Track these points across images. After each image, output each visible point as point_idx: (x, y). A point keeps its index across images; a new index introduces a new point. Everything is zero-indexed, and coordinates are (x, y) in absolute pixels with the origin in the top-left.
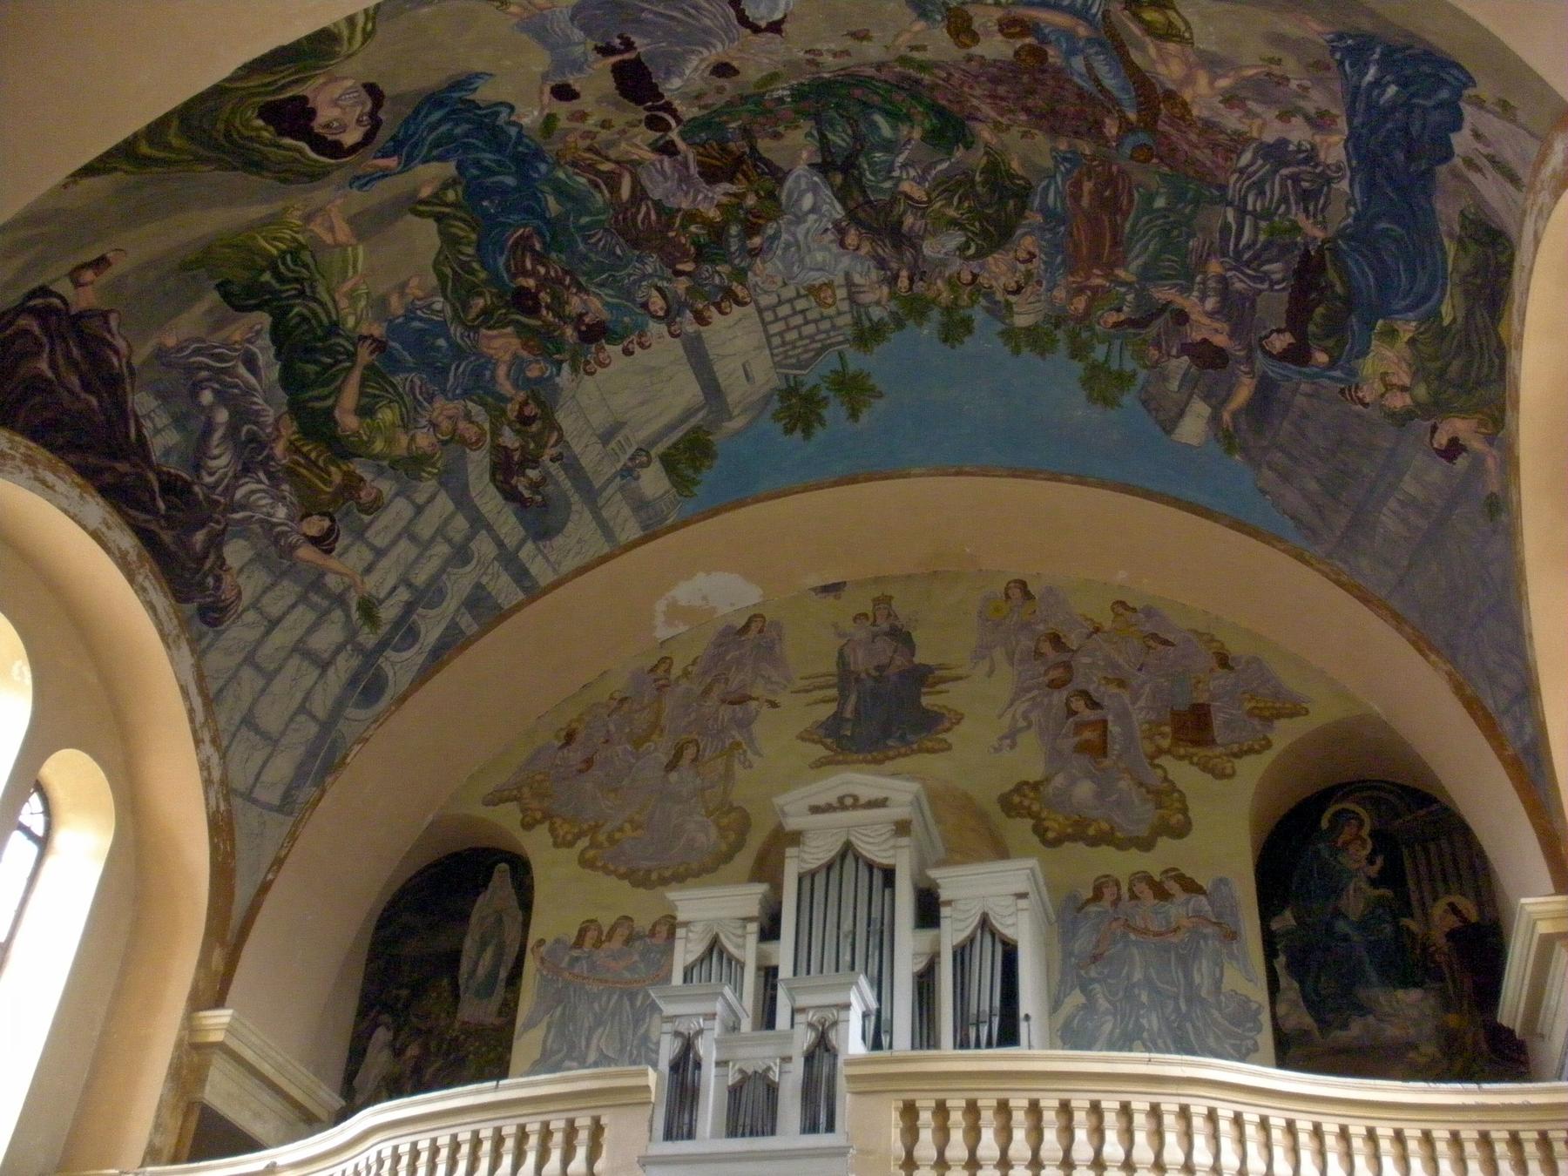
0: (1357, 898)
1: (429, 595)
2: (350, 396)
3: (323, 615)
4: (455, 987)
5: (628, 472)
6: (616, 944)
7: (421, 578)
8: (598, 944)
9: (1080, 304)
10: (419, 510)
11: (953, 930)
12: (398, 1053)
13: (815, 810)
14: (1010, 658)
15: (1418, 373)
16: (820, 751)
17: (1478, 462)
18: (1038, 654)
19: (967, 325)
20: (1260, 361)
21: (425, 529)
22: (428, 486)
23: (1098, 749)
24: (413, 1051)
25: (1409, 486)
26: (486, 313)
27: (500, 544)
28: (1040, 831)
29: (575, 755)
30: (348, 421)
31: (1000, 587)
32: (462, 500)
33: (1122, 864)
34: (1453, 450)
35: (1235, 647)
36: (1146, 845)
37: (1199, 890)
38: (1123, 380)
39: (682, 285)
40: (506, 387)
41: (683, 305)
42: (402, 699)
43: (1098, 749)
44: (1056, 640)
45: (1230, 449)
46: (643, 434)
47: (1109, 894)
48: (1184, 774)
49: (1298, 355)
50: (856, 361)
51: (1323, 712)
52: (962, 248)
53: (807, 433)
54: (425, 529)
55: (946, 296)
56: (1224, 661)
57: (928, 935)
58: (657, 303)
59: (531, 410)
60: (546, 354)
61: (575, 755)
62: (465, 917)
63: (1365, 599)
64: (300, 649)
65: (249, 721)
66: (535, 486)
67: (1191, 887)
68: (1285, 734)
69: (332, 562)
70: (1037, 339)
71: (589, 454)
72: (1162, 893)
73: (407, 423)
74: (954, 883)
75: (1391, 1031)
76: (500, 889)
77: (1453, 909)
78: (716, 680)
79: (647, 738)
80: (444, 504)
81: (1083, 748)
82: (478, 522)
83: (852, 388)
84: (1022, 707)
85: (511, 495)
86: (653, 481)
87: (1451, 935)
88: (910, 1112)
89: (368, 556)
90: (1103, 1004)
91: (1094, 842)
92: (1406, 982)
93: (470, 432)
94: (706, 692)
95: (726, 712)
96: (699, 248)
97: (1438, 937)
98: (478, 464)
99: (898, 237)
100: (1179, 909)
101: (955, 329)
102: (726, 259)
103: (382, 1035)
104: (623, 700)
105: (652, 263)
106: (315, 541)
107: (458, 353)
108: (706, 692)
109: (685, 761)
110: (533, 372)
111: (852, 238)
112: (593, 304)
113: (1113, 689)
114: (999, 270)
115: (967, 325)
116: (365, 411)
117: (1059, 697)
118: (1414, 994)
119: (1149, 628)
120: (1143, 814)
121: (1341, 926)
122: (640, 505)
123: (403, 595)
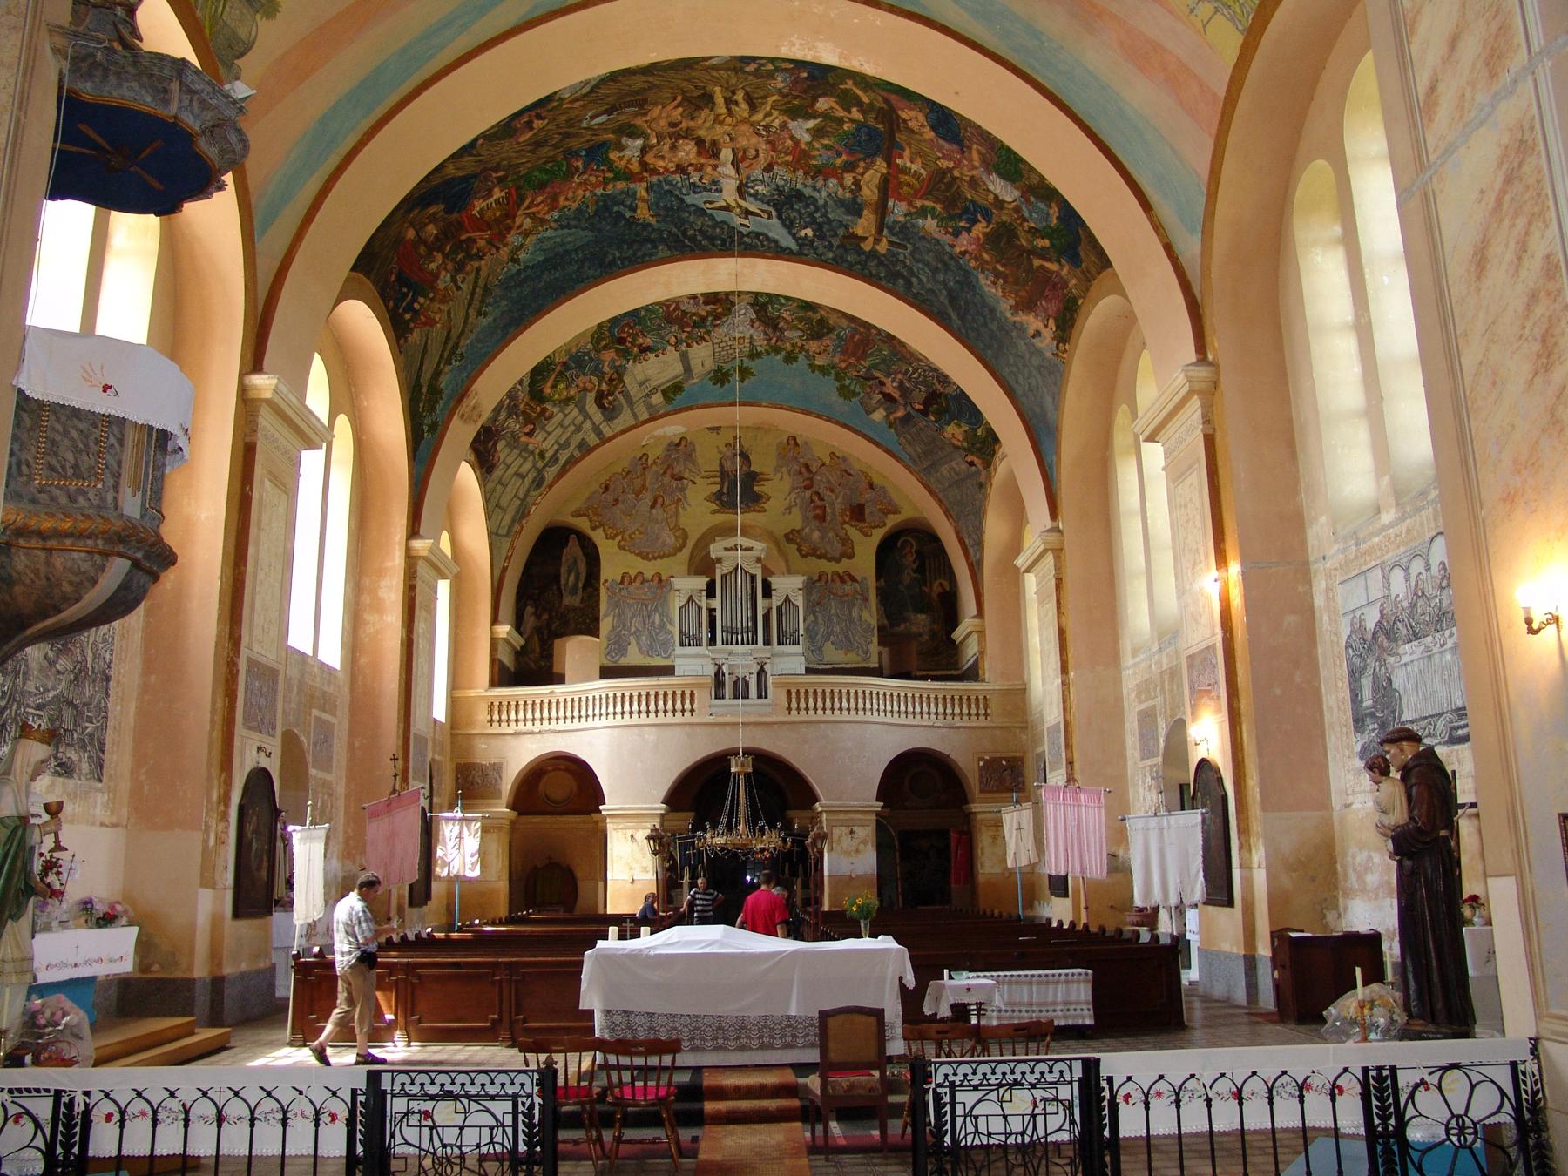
0: (908, 576)
1: (564, 446)
2: (549, 384)
3: (525, 459)
4: (559, 588)
5: (648, 396)
6: (638, 583)
7: (562, 440)
8: (630, 583)
9: (844, 365)
10: (566, 415)
11: (776, 601)
12: (538, 618)
13: (726, 549)
14: (789, 472)
15: (965, 439)
16: (714, 507)
17: (978, 472)
18: (800, 473)
19: (795, 359)
20: (909, 407)
21: (566, 423)
22: (571, 406)
23: (821, 518)
24: (545, 617)
25: (953, 464)
26: (605, 346)
27: (594, 424)
28: (799, 550)
29: (610, 497)
30: (547, 390)
31: (785, 438)
32: (582, 410)
33: (829, 567)
34: (971, 464)
35: (877, 481)
36: (838, 560)
37: (856, 581)
38: (854, 394)
39: (684, 335)
40: (606, 369)
41: (682, 341)
42: (550, 486)
43: (821, 518)
44: (807, 467)
45: (890, 427)
46: (656, 383)
47: (824, 578)
48: (853, 533)
49: (925, 413)
50: (747, 363)
51: (906, 514)
52: (800, 337)
53: (722, 385)
54: (566, 423)
55: (789, 348)
56: (871, 486)
57: (767, 601)
58: (673, 340)
59: (615, 376)
60: (625, 357)
61: (610, 497)
62: (560, 558)
63: (930, 492)
64: (517, 474)
65: (497, 505)
66: (610, 403)
67: (853, 579)
68: (892, 521)
69: (532, 440)
70: (824, 370)
71: (633, 389)
72: (843, 581)
73: (567, 388)
74: (775, 582)
75: (914, 629)
76: (573, 549)
77: (941, 584)
78: (669, 467)
79: (641, 492)
80: (576, 412)
81: (816, 517)
82: (587, 416)
83: (745, 372)
84: (793, 496)
85: (600, 406)
86: (657, 399)
87: (939, 595)
88: (789, 693)
89: (545, 435)
90: (820, 621)
91: (820, 557)
92: (921, 612)
93: (589, 386)
94: (665, 473)
95: (674, 483)
96: (694, 323)
97: (934, 596)
98: (591, 396)
99: (775, 327)
100: (848, 587)
101: (790, 359)
102: (705, 327)
103: (529, 610)
104: (628, 473)
105: (675, 328)
106: (527, 434)
107: (591, 360)
108: (665, 473)
109: (659, 505)
110: (617, 364)
111: (757, 324)
112: (648, 341)
113: (829, 493)
114: (813, 346)
115: (795, 359)
116: (554, 386)
117: (808, 494)
118: (924, 616)
119: (843, 467)
120: (837, 548)
121: (900, 587)
122: (650, 407)
123: (556, 447)
